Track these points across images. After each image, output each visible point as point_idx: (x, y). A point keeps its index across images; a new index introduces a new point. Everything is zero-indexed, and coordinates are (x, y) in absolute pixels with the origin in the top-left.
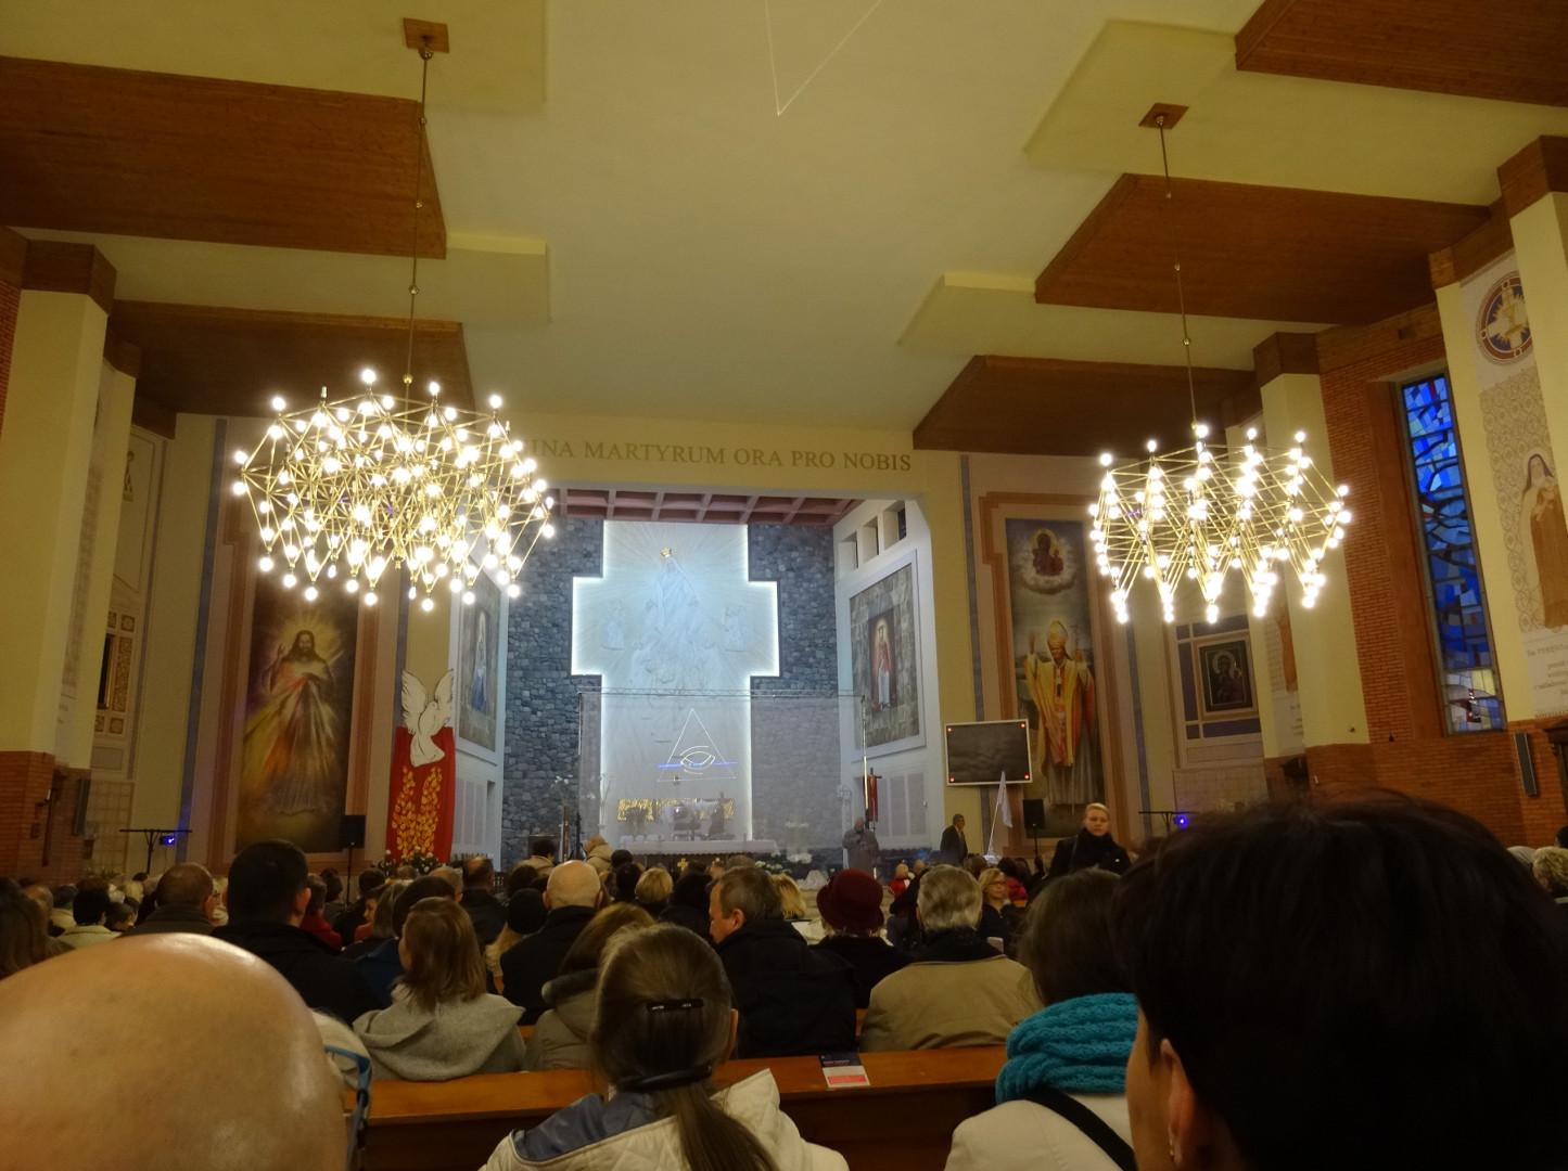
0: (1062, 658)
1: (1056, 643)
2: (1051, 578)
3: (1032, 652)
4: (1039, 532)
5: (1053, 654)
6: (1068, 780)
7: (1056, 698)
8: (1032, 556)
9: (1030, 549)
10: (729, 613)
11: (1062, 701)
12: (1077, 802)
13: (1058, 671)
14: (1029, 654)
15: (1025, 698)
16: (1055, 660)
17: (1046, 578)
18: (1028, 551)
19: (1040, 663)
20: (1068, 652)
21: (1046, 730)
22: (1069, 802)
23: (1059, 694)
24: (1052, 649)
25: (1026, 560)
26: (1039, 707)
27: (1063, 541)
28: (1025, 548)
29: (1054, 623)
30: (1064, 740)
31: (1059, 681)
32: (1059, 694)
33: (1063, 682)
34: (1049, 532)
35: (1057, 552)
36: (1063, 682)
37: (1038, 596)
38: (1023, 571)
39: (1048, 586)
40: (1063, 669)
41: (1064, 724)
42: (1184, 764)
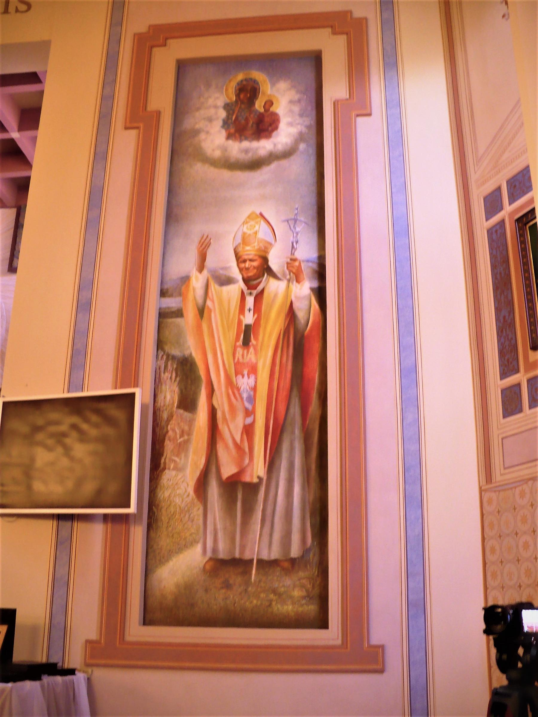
0: (259, 276)
1: (250, 251)
2: (255, 144)
3: (201, 268)
4: (240, 77)
5: (241, 270)
6: (248, 511)
7: (240, 351)
8: (223, 114)
9: (220, 103)
10: (497, 493)
11: (251, 356)
12: (265, 556)
13: (250, 301)
14: (194, 274)
15: (176, 352)
16: (246, 281)
17: (246, 144)
18: (216, 107)
19: (214, 287)
20: (274, 263)
21: (213, 413)
22: (247, 556)
23: (246, 343)
24: (239, 259)
25: (210, 120)
26: (202, 373)
27: (283, 85)
28: (211, 101)
29: (250, 217)
30: (248, 430)
31: (249, 319)
32: (246, 343)
33: (257, 322)
34: (258, 76)
35: (269, 103)
36: (257, 322)
37: (226, 174)
38: (202, 136)
39: (248, 157)
40: (259, 298)
41: (252, 399)
42: (498, 476)
